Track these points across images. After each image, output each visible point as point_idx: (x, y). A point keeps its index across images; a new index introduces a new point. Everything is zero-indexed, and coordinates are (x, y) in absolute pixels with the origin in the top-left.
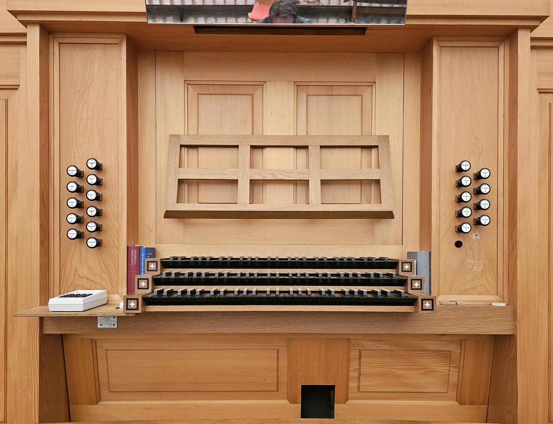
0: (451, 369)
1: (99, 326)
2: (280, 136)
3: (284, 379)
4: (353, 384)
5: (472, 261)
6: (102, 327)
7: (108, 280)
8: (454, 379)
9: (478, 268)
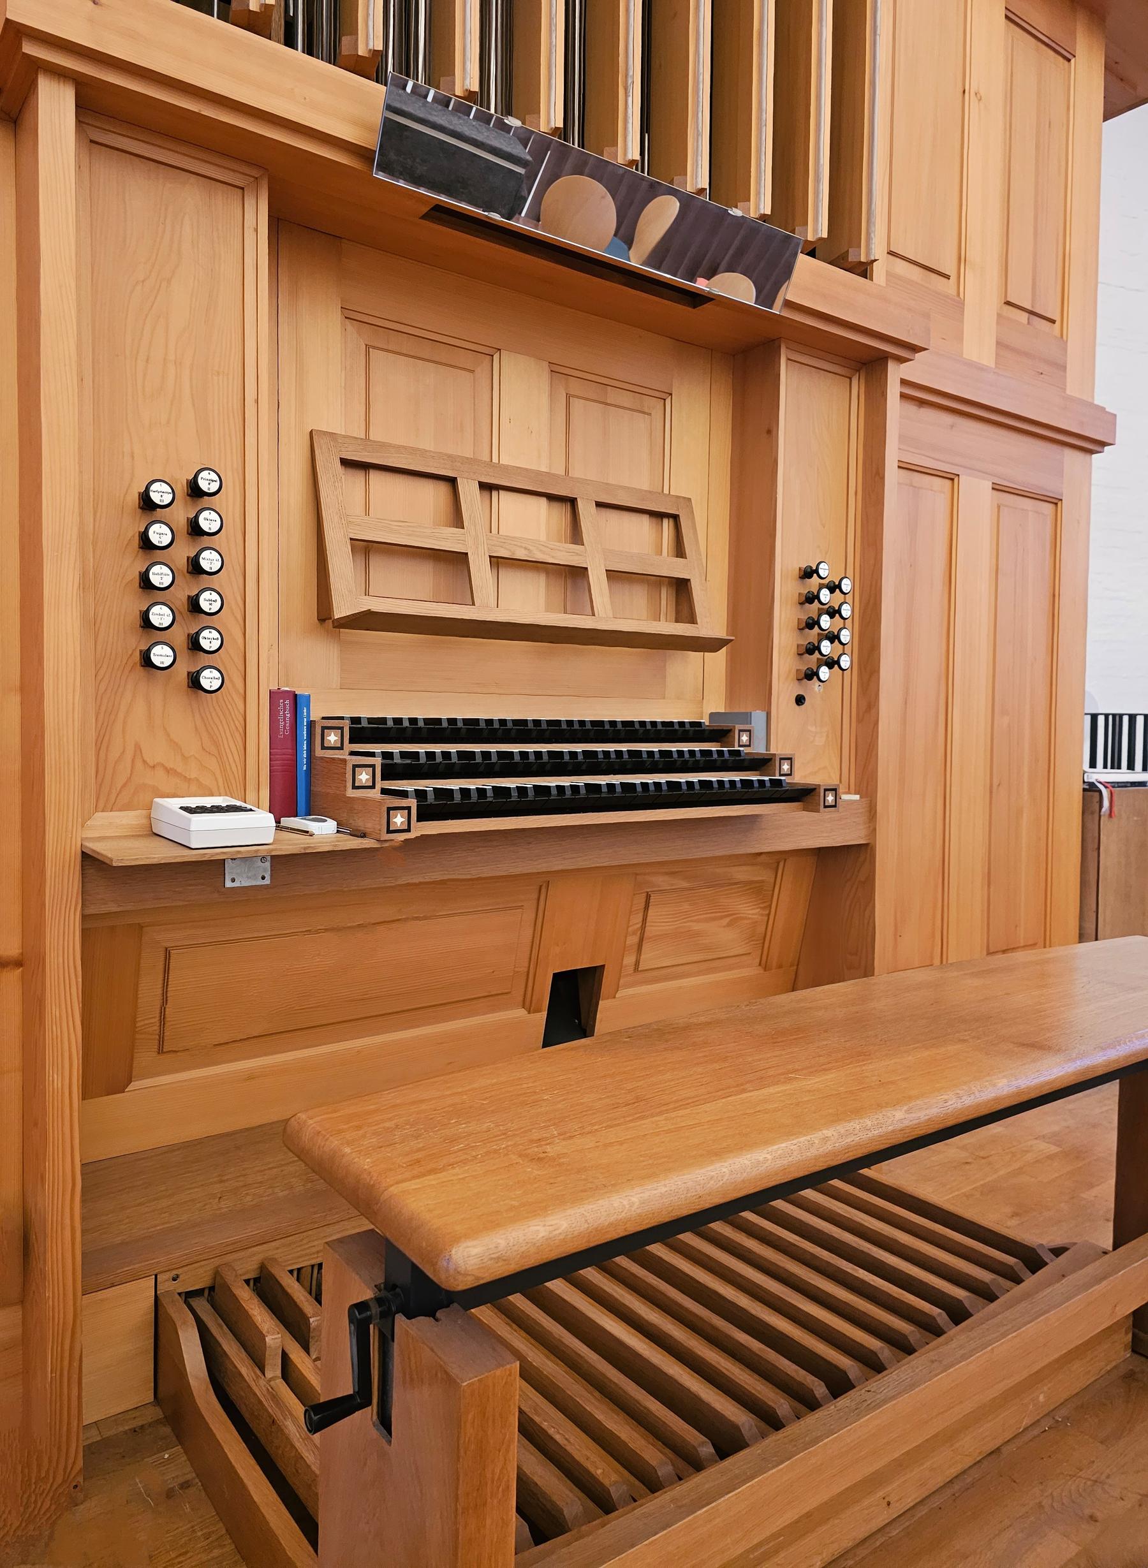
1: (228, 884)
2: (526, 470)
5: (813, 729)
6: (236, 884)
7: (218, 773)
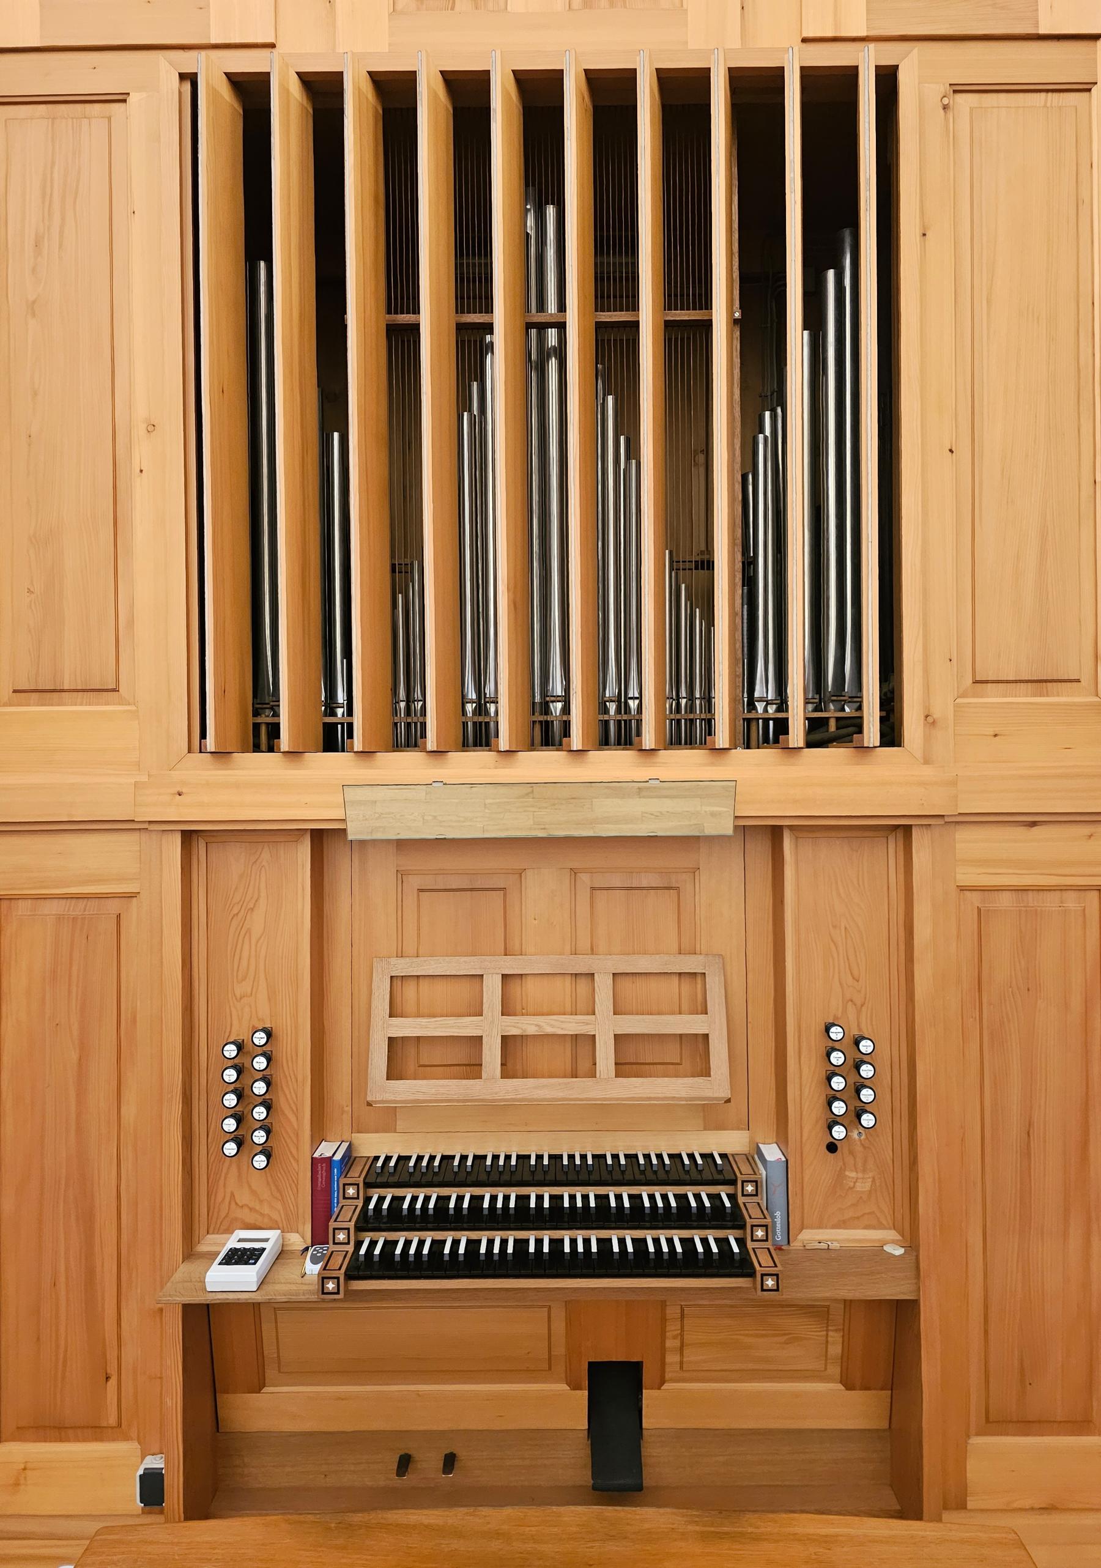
0: (831, 1333)
3: (560, 1350)
4: (672, 1359)
5: (853, 1175)
8: (835, 1350)
9: (864, 1186)
